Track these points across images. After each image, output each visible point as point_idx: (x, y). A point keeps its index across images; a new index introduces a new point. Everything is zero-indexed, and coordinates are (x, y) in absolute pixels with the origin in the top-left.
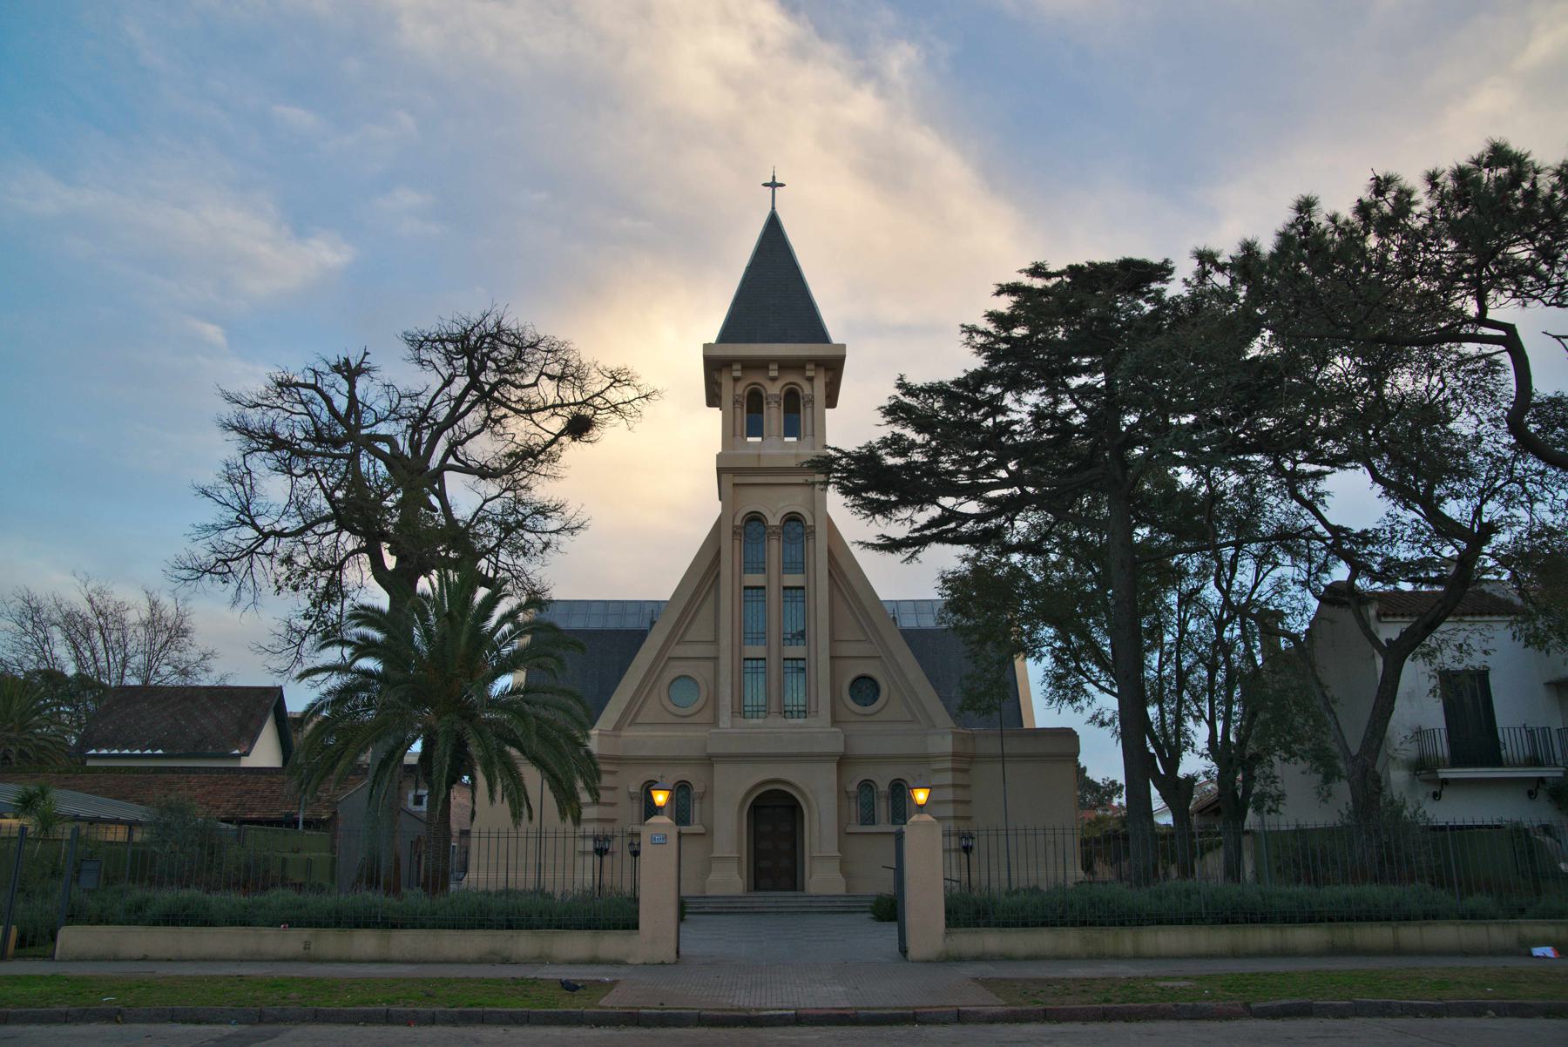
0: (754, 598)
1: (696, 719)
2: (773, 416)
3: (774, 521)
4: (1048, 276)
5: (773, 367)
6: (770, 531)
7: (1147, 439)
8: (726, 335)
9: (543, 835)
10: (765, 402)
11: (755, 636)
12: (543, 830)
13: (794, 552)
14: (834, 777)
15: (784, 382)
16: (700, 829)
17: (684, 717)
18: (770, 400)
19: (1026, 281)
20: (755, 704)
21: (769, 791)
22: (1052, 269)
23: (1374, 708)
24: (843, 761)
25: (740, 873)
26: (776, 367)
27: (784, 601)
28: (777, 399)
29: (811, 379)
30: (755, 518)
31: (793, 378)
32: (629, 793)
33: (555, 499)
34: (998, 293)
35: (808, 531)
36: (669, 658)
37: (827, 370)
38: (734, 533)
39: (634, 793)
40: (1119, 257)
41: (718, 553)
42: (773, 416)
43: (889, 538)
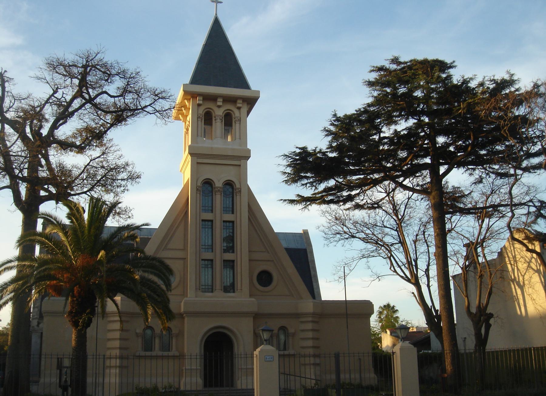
3: (219, 184)
4: (399, 63)
5: (239, 101)
6: (216, 189)
8: (195, 80)
9: (98, 357)
10: (214, 119)
11: (206, 247)
12: (98, 354)
13: (228, 202)
14: (251, 324)
15: (223, 110)
16: (177, 354)
18: (217, 118)
19: (387, 65)
20: (206, 284)
21: (215, 333)
22: (402, 60)
26: (221, 100)
28: (221, 118)
29: (239, 108)
30: (208, 183)
31: (230, 107)
32: (136, 333)
33: (282, 169)
34: (372, 71)
35: (237, 191)
37: (248, 104)
38: (197, 190)
40: (434, 58)
42: (218, 126)
43: (301, 196)
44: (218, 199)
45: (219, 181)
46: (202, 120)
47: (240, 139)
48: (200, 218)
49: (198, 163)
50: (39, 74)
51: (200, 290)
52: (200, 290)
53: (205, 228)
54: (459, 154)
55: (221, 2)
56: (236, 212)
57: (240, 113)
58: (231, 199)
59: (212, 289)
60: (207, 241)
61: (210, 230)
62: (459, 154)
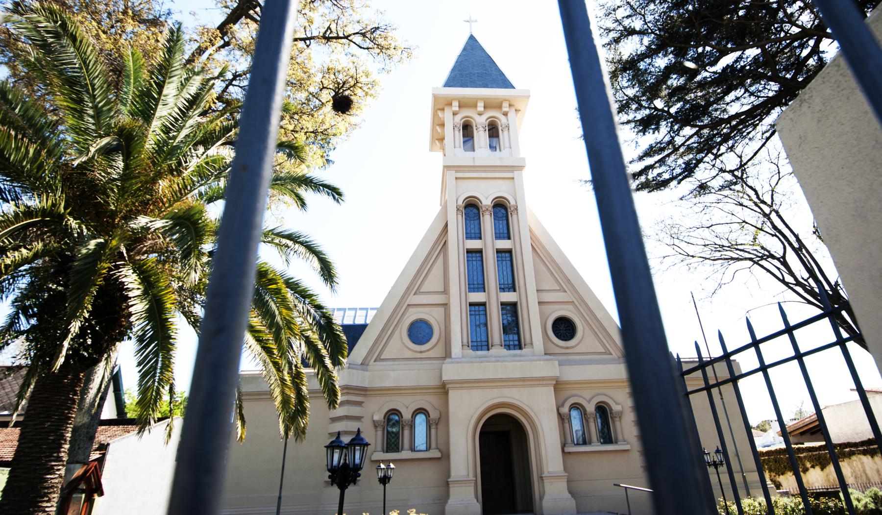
0: (504, 259)
1: (430, 354)
2: (481, 137)
3: (486, 201)
7: (171, 140)
10: (475, 128)
13: (501, 226)
17: (421, 352)
23: (589, 364)
24: (558, 386)
25: (477, 498)
26: (482, 104)
27: (498, 261)
29: (506, 114)
32: (374, 421)
36: (408, 305)
38: (458, 210)
39: (378, 421)
41: (446, 225)
42: (481, 137)
44: (488, 222)
45: (487, 199)
46: (460, 130)
47: (510, 148)
48: (464, 247)
49: (456, 178)
50: (168, 97)
51: (468, 346)
52: (468, 346)
53: (472, 261)
54: (876, 446)
55: (476, 21)
56: (519, 287)
57: (508, 120)
58: (505, 222)
59: (488, 345)
60: (475, 278)
61: (479, 263)
62: (876, 446)
